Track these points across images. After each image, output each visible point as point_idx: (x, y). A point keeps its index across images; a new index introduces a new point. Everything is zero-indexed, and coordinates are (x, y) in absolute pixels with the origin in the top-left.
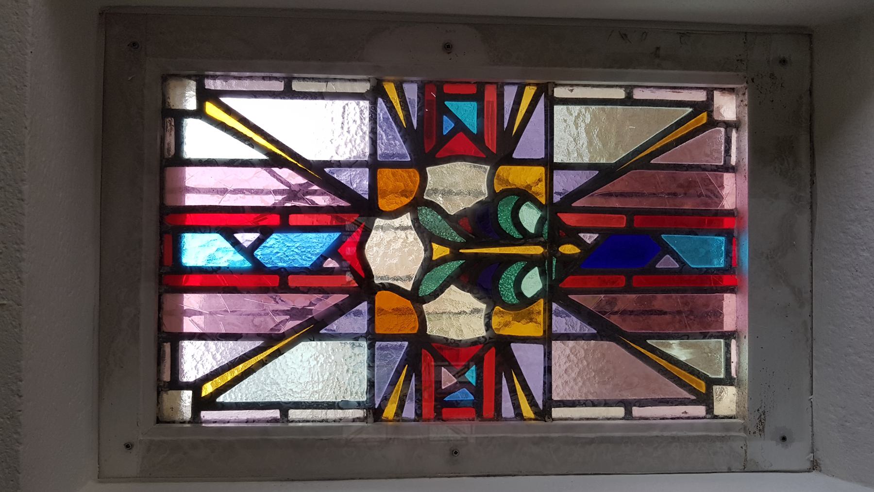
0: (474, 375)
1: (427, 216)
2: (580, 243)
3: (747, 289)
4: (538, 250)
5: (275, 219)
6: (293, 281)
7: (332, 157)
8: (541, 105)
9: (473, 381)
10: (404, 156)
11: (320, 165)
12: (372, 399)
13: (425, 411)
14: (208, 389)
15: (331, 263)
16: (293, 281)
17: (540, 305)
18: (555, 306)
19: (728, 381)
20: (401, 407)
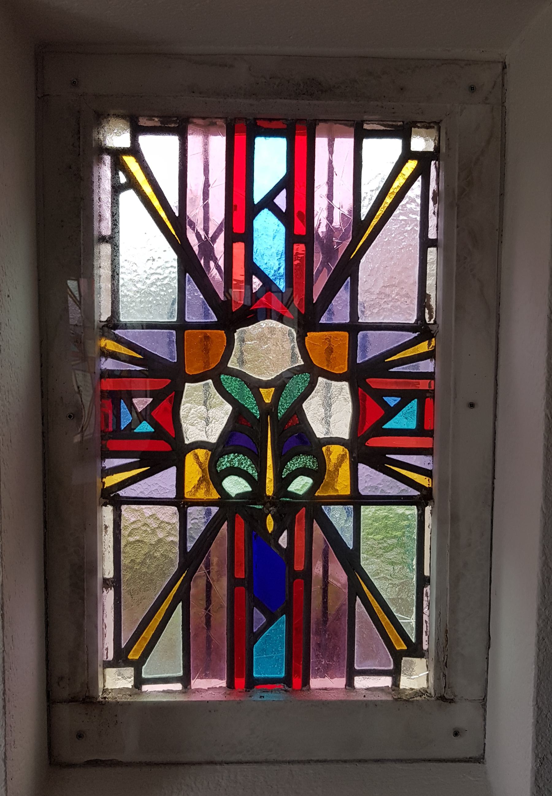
0: (144, 430)
1: (302, 381)
2: (278, 533)
3: (232, 698)
4: (270, 489)
5: (300, 229)
6: (239, 248)
7: (174, 259)
10: (364, 356)
12: (125, 326)
14: (130, 161)
16: (239, 248)
17: (215, 495)
18: (323, 320)
19: (139, 682)
20: (114, 355)
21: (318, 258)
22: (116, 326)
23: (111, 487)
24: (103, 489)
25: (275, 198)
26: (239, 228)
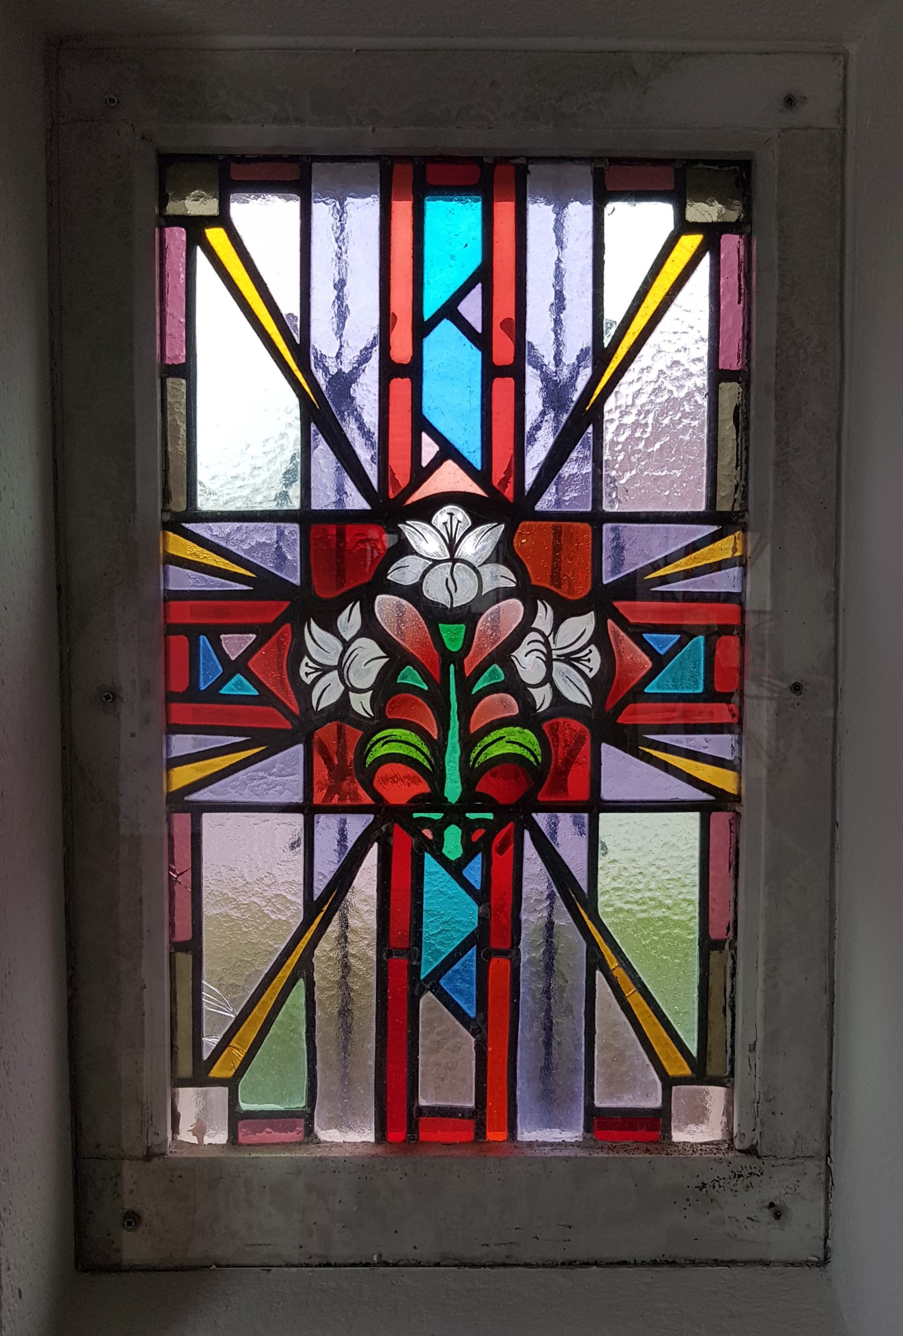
5: (503, 353)
6: (401, 387)
8: (704, 796)
9: (227, 690)
10: (618, 564)
11: (311, 907)
13: (727, 719)
15: (429, 449)
21: (534, 403)
22: (704, 809)
23: (179, 790)
24: (168, 794)
25: (458, 304)
26: (402, 352)
